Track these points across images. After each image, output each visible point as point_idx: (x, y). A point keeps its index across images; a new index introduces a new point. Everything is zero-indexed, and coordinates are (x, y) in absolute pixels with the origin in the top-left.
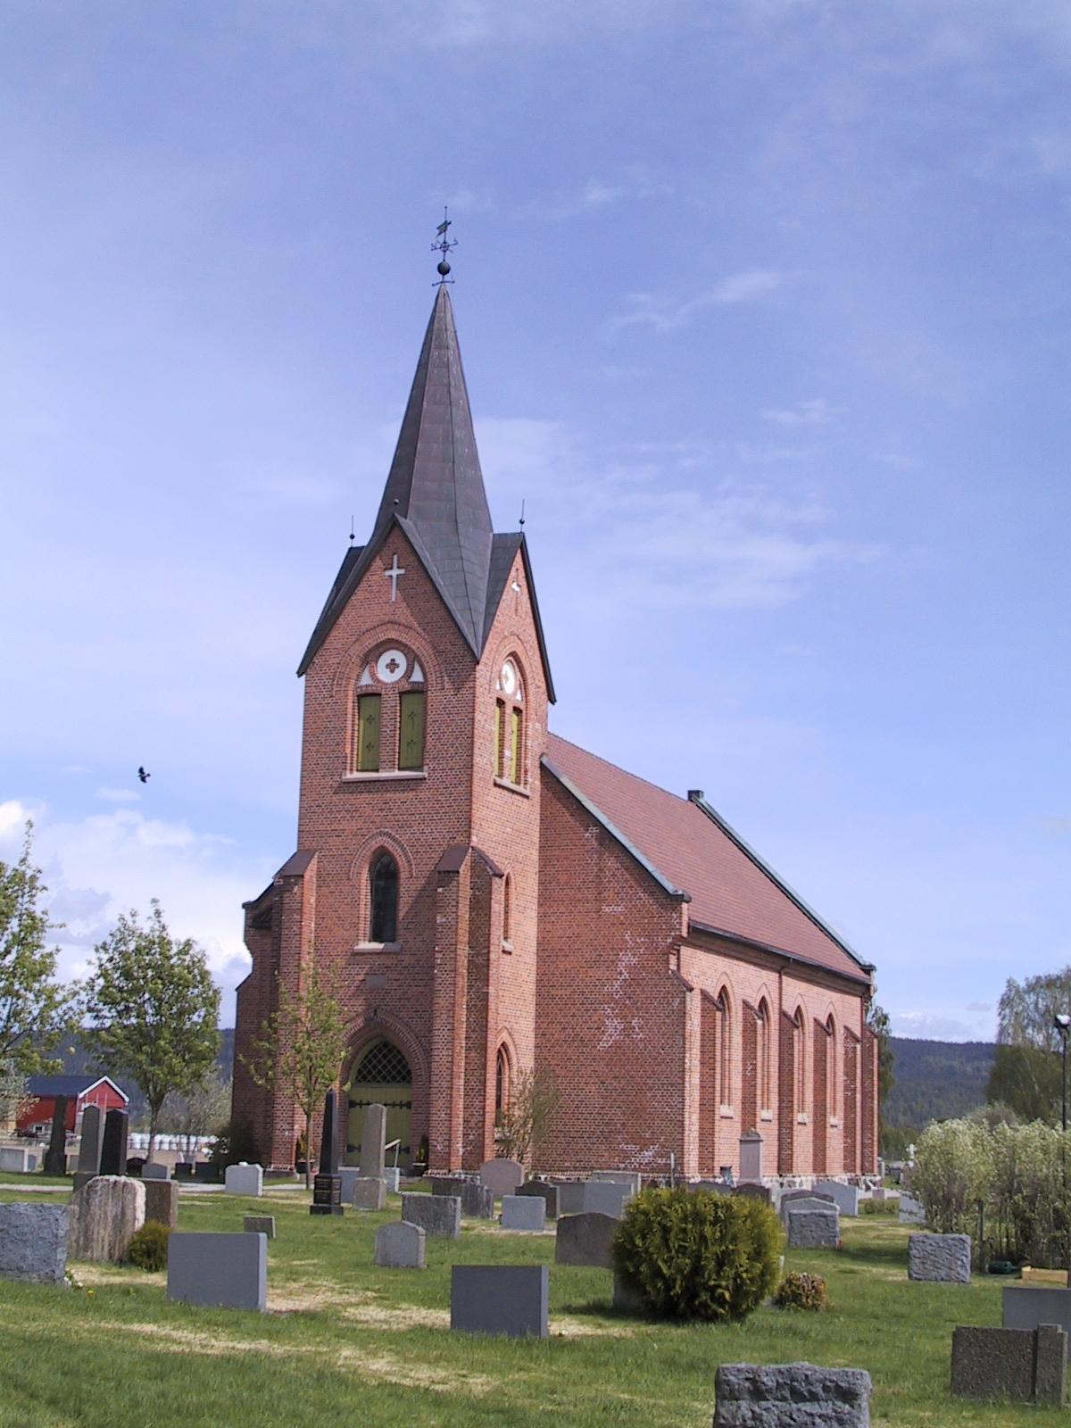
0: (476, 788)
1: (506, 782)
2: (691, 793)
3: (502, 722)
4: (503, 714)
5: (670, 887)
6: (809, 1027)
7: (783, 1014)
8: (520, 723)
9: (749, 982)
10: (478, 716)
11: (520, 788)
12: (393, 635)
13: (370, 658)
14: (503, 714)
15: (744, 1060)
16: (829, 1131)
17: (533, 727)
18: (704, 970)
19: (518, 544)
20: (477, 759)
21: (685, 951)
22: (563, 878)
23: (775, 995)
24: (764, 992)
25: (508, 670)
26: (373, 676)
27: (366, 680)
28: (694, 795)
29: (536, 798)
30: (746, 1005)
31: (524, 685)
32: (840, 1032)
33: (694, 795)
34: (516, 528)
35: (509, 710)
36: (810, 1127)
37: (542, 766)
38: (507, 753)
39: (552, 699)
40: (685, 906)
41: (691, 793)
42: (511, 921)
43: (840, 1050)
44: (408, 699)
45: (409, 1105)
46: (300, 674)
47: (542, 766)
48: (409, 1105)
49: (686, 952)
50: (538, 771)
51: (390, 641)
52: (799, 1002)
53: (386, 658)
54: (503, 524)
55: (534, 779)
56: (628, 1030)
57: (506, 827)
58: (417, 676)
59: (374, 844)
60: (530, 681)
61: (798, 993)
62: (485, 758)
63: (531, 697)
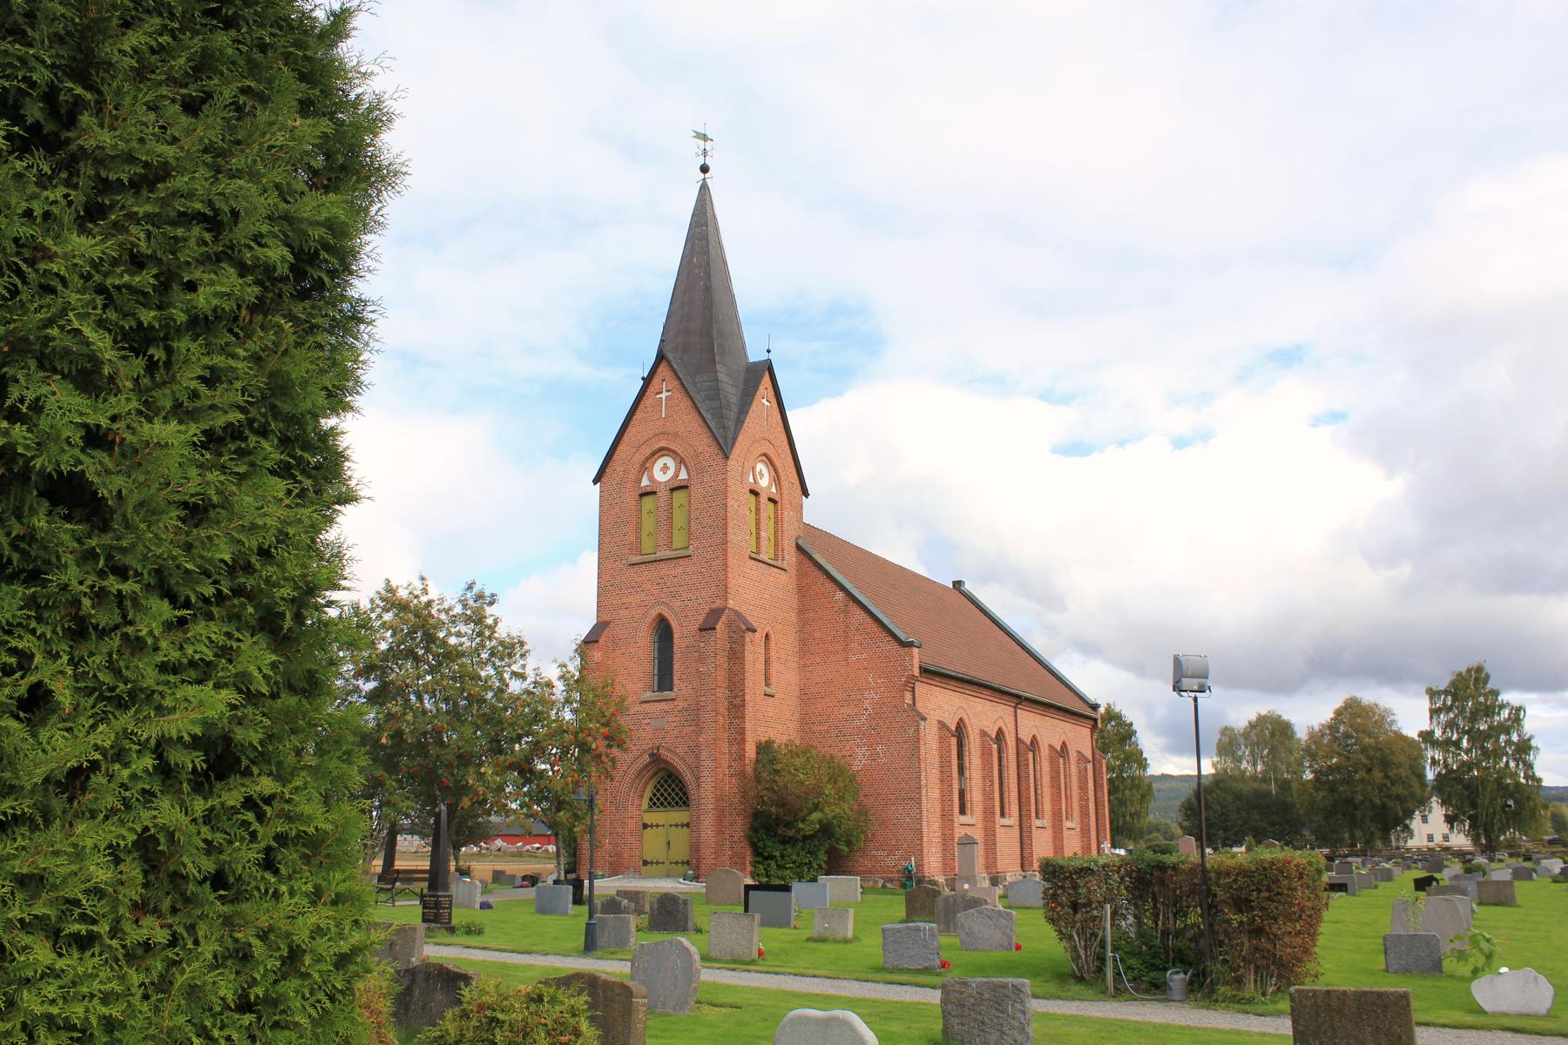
0: (732, 562)
1: (763, 557)
2: (955, 583)
3: (758, 510)
4: (758, 503)
5: (903, 637)
6: (1045, 751)
7: (1018, 740)
8: (776, 512)
9: (985, 715)
10: (730, 502)
11: (779, 563)
12: (664, 444)
13: (645, 466)
14: (758, 503)
15: (984, 778)
16: (1066, 833)
17: (788, 514)
18: (940, 704)
19: (768, 367)
20: (731, 537)
21: (921, 689)
22: (818, 634)
23: (1011, 726)
24: (1000, 724)
25: (760, 467)
26: (651, 478)
27: (645, 482)
28: (958, 584)
29: (793, 571)
30: (984, 734)
31: (777, 479)
32: (1073, 755)
33: (958, 584)
34: (764, 357)
35: (763, 499)
36: (1049, 832)
37: (799, 547)
38: (763, 534)
39: (805, 493)
40: (916, 650)
41: (955, 583)
42: (773, 671)
43: (1074, 769)
44: (676, 494)
45: (688, 825)
46: (595, 482)
47: (799, 547)
48: (688, 825)
49: (921, 689)
50: (793, 550)
51: (662, 449)
52: (1034, 732)
53: (660, 463)
54: (755, 354)
55: (790, 558)
56: (874, 757)
57: (760, 593)
58: (683, 475)
59: (654, 613)
60: (783, 478)
61: (1032, 724)
62: (740, 538)
63: (785, 492)
